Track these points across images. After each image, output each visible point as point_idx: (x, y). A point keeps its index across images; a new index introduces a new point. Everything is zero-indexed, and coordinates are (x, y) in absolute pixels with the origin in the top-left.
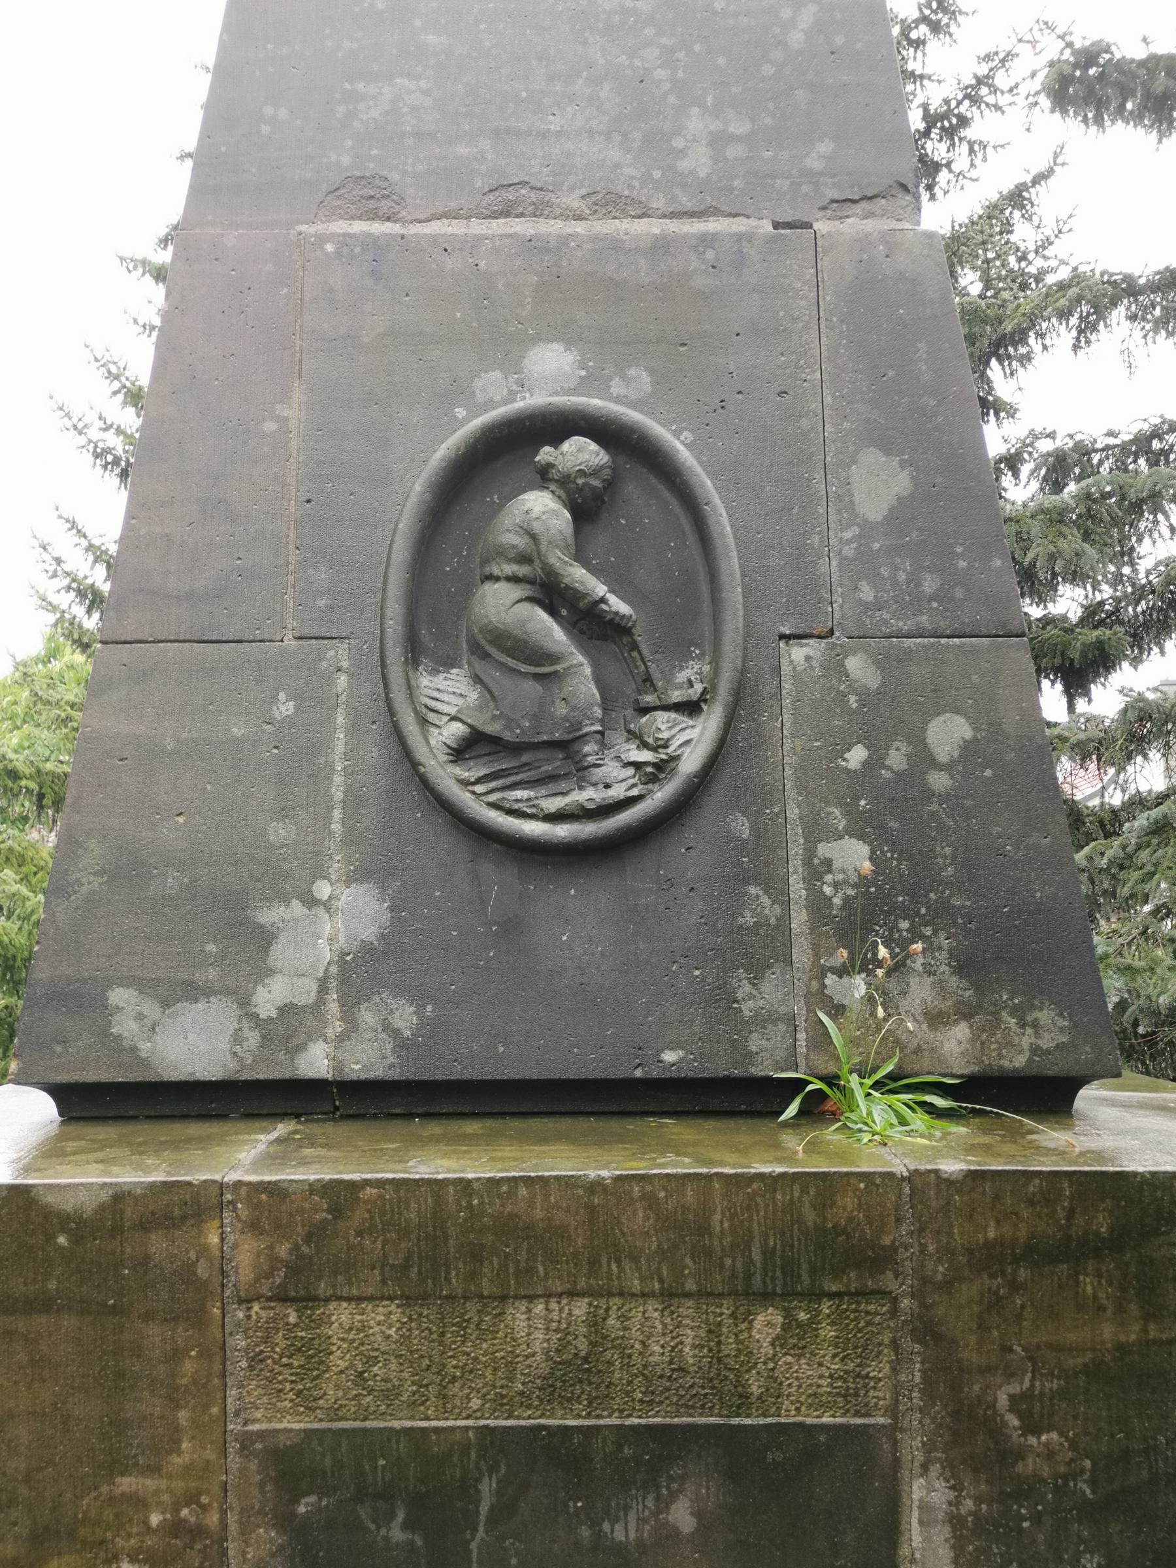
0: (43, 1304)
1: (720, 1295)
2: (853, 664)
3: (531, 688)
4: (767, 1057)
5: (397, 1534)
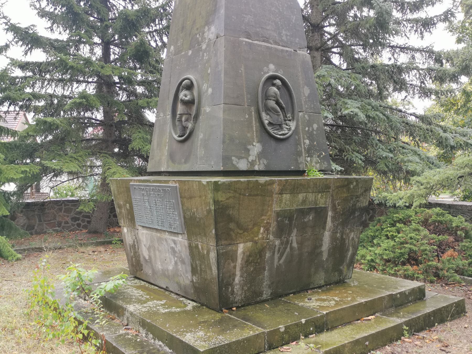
0: (257, 195)
1: (178, 234)
2: (306, 116)
3: (276, 116)
4: (302, 168)
5: (287, 222)
